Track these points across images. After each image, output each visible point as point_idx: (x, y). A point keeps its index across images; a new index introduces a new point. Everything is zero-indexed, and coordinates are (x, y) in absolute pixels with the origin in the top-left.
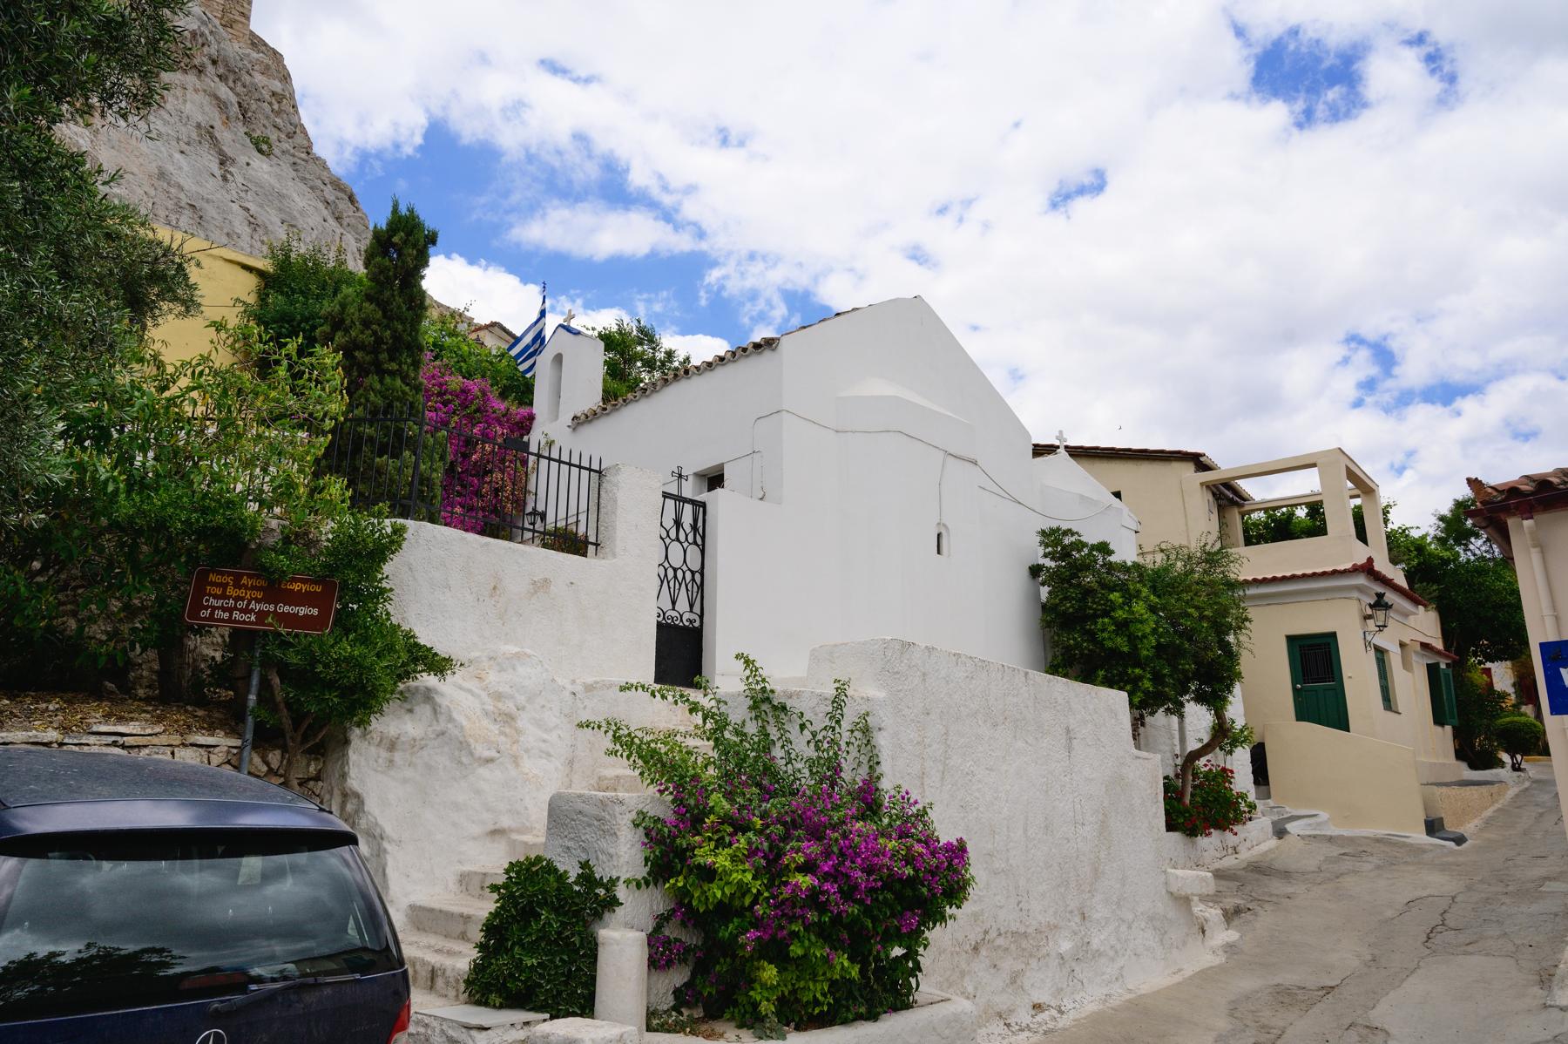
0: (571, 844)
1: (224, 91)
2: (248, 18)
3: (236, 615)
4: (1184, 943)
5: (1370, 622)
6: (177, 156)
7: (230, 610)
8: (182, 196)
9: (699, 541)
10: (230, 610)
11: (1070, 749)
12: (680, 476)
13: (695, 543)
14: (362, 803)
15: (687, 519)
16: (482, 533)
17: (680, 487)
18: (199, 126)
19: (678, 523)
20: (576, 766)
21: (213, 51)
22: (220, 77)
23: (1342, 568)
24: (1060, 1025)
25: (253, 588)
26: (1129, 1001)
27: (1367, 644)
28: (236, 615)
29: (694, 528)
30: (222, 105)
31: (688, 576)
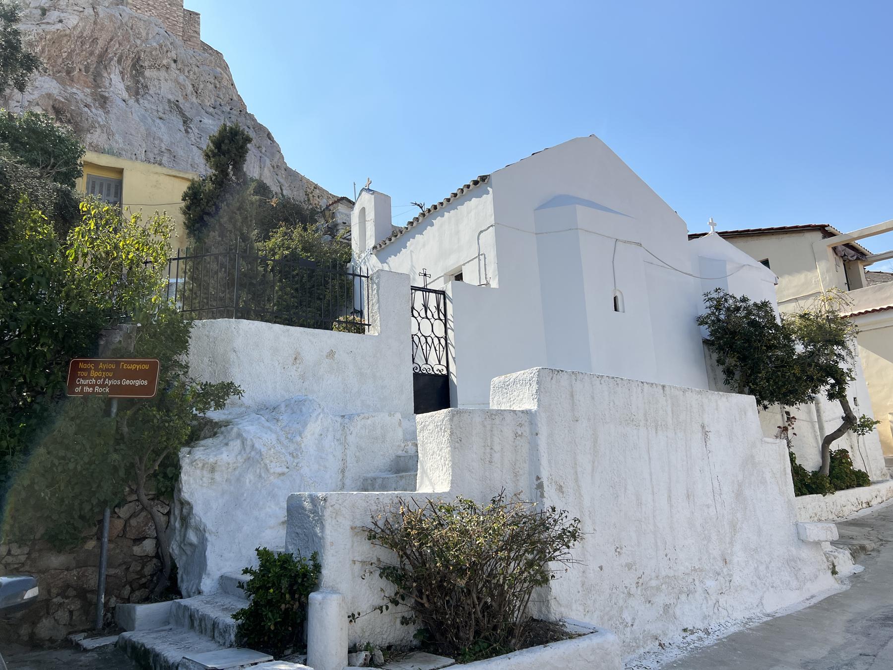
0: (299, 531)
3: (97, 389)
4: (816, 577)
6: (158, 121)
7: (93, 386)
9: (442, 317)
10: (93, 386)
12: (425, 275)
14: (191, 508)
15: (432, 304)
18: (169, 101)
19: (426, 307)
20: (346, 474)
24: (706, 643)
25: (107, 370)
26: (766, 623)
28: (97, 389)
29: (438, 308)
30: (182, 87)
31: (436, 341)
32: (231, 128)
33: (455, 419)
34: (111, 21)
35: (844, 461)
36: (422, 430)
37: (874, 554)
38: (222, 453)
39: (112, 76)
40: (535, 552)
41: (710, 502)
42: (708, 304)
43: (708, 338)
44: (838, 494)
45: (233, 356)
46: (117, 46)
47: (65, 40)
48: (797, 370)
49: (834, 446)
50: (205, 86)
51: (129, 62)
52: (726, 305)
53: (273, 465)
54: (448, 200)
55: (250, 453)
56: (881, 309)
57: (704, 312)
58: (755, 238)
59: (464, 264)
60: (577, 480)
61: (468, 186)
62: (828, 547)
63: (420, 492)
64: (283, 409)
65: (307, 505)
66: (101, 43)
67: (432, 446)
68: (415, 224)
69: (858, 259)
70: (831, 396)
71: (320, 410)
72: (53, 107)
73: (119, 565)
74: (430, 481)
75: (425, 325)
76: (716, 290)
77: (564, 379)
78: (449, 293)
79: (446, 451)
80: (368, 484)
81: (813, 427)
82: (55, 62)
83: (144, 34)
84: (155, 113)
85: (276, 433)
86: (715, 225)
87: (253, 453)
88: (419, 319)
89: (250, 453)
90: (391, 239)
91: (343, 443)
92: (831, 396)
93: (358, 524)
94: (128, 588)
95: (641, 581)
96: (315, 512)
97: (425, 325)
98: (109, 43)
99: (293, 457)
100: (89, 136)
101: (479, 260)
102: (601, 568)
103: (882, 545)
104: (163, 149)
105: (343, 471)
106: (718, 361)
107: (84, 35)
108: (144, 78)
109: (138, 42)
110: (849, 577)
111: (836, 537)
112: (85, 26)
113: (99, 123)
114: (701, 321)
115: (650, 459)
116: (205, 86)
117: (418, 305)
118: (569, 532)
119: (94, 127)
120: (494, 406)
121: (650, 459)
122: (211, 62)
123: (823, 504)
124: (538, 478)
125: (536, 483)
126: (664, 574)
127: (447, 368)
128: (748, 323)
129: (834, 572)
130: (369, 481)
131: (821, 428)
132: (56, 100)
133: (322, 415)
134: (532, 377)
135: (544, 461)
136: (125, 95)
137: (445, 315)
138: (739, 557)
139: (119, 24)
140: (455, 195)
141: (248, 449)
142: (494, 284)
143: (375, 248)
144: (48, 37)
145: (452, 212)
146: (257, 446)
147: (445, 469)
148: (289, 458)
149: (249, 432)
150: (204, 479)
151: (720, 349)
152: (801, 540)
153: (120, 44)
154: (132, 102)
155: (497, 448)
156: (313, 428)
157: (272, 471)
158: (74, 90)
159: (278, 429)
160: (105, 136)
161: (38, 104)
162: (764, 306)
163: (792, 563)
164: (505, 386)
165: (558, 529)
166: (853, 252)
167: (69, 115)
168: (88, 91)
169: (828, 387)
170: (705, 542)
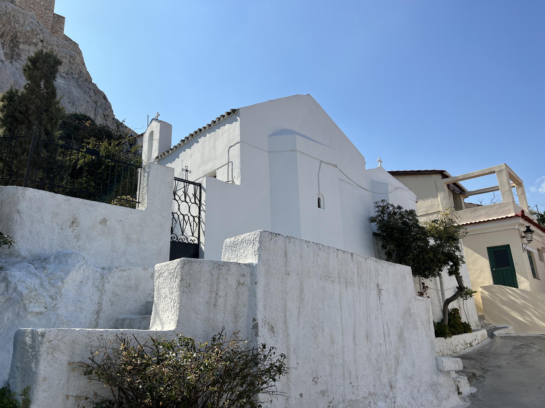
4: (449, 397)
5: (525, 239)
9: (197, 202)
11: (346, 288)
12: (187, 171)
13: (195, 203)
16: (67, 194)
19: (186, 194)
20: (101, 315)
23: (510, 216)
27: (524, 249)
29: (195, 195)
32: (46, 53)
33: (186, 267)
35: (456, 316)
36: (159, 277)
37: (481, 379)
40: (244, 386)
41: (382, 341)
42: (377, 209)
43: (377, 232)
44: (454, 337)
45: (16, 216)
48: (431, 255)
49: (451, 306)
51: (9, 37)
52: (388, 211)
53: (31, 305)
54: (210, 125)
55: (12, 294)
56: (475, 223)
57: (374, 214)
58: (403, 176)
59: (218, 169)
60: (285, 322)
61: (224, 116)
62: (454, 375)
63: (151, 330)
64: (52, 259)
65: (28, 340)
67: (165, 291)
68: (185, 142)
69: (461, 193)
70: (450, 273)
71: (83, 262)
74: (161, 320)
75: (184, 206)
76: (382, 201)
77: (280, 241)
78: (204, 185)
79: (176, 294)
80: (118, 323)
81: (438, 293)
83: (22, 22)
85: (40, 278)
86: (382, 162)
87: (14, 294)
88: (180, 202)
89: (12, 294)
90: (168, 153)
91: (101, 291)
92: (450, 273)
93: (77, 359)
95: (331, 405)
96: (33, 347)
97: (184, 206)
99: (53, 299)
101: (228, 166)
102: (301, 395)
103: (484, 373)
105: (98, 313)
106: (382, 246)
108: (18, 48)
109: (17, 26)
110: (468, 396)
111: (461, 368)
114: (372, 220)
115: (341, 307)
117: (180, 193)
118: (276, 366)
120: (224, 259)
121: (341, 307)
122: (69, 47)
123: (445, 344)
124: (254, 320)
125: (253, 324)
126: (349, 398)
127: (199, 239)
128: (402, 223)
129: (459, 393)
130: (120, 322)
131: (443, 294)
133: (84, 266)
134: (256, 238)
135: (260, 306)
137: (200, 201)
138: (400, 383)
139: (4, 12)
140: (214, 122)
141: (10, 291)
142: (238, 182)
143: (157, 157)
145: (212, 133)
146: (20, 288)
147: (173, 311)
148: (48, 300)
149: (14, 277)
151: (384, 238)
152: (440, 370)
154: (7, 62)
155: (221, 293)
156: (75, 276)
157: (30, 310)
159: (43, 276)
162: (412, 213)
163: (434, 387)
164: (234, 246)
165: (267, 364)
166: (458, 189)
169: (449, 267)
170: (378, 372)
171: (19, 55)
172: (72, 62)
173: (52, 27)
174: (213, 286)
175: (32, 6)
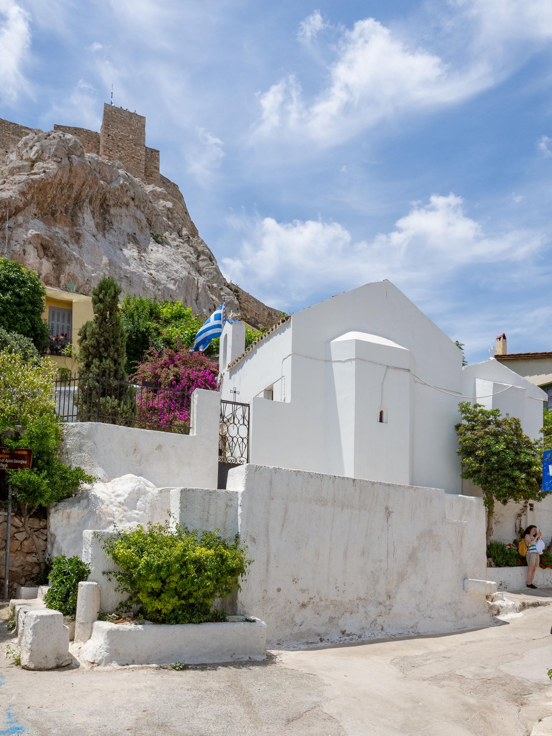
1: (139, 214)
2: (158, 169)
8: (122, 272)
9: (246, 423)
12: (235, 392)
17: (235, 397)
18: (128, 234)
21: (131, 193)
22: (137, 206)
25: (6, 454)
29: (244, 417)
30: (138, 221)
34: (83, 168)
38: (75, 507)
39: (85, 215)
46: (88, 189)
47: (49, 187)
50: (157, 219)
51: (98, 202)
60: (267, 536)
66: (76, 188)
72: (42, 245)
73: (19, 566)
82: (42, 206)
83: (109, 177)
84: (117, 246)
94: (24, 579)
95: (312, 601)
98: (82, 187)
100: (67, 267)
104: (122, 276)
107: (63, 182)
108: (109, 214)
112: (63, 174)
113: (74, 256)
116: (157, 219)
119: (70, 260)
132: (43, 239)
136: (95, 231)
144: (36, 185)
145: (271, 340)
150: (64, 521)
153: (91, 187)
154: (100, 236)
155: (212, 512)
158: (57, 230)
160: (78, 267)
161: (30, 243)
167: (53, 251)
168: (67, 229)
171: (111, 223)
172: (170, 216)
173: (146, 168)
174: (205, 507)
175: (120, 144)
